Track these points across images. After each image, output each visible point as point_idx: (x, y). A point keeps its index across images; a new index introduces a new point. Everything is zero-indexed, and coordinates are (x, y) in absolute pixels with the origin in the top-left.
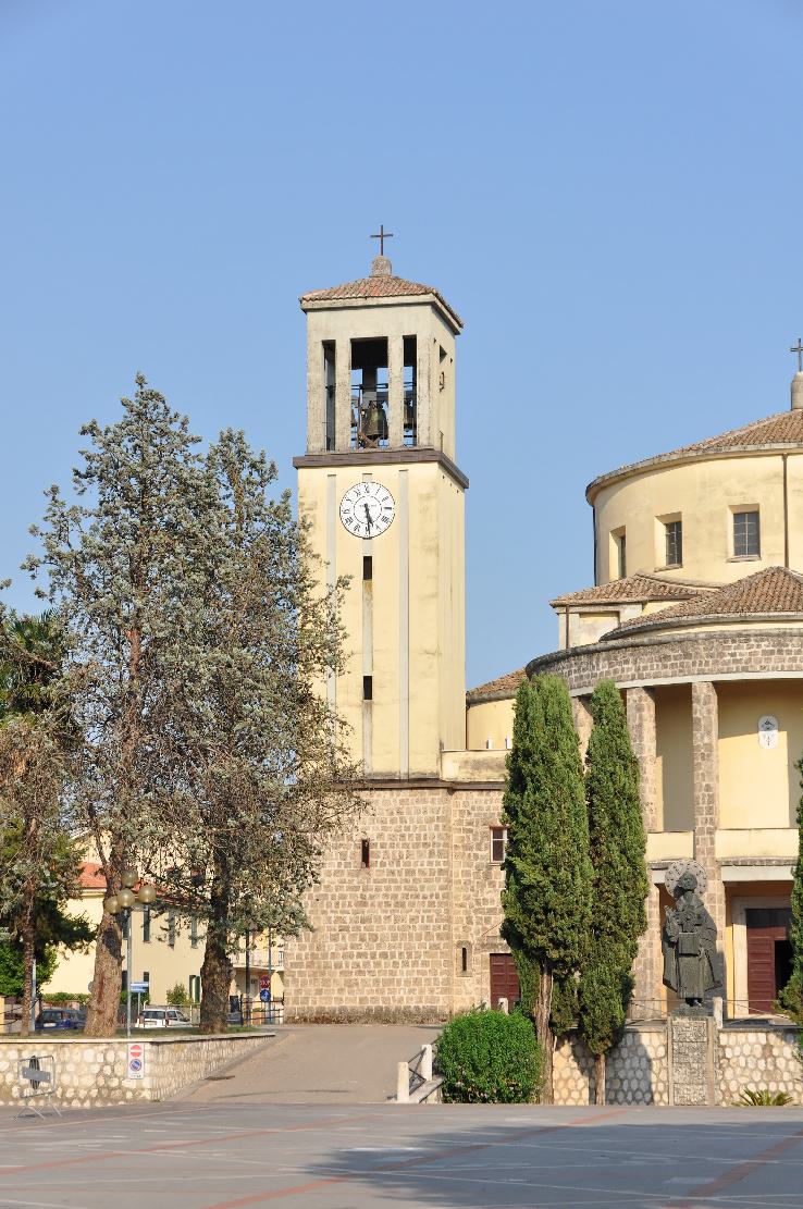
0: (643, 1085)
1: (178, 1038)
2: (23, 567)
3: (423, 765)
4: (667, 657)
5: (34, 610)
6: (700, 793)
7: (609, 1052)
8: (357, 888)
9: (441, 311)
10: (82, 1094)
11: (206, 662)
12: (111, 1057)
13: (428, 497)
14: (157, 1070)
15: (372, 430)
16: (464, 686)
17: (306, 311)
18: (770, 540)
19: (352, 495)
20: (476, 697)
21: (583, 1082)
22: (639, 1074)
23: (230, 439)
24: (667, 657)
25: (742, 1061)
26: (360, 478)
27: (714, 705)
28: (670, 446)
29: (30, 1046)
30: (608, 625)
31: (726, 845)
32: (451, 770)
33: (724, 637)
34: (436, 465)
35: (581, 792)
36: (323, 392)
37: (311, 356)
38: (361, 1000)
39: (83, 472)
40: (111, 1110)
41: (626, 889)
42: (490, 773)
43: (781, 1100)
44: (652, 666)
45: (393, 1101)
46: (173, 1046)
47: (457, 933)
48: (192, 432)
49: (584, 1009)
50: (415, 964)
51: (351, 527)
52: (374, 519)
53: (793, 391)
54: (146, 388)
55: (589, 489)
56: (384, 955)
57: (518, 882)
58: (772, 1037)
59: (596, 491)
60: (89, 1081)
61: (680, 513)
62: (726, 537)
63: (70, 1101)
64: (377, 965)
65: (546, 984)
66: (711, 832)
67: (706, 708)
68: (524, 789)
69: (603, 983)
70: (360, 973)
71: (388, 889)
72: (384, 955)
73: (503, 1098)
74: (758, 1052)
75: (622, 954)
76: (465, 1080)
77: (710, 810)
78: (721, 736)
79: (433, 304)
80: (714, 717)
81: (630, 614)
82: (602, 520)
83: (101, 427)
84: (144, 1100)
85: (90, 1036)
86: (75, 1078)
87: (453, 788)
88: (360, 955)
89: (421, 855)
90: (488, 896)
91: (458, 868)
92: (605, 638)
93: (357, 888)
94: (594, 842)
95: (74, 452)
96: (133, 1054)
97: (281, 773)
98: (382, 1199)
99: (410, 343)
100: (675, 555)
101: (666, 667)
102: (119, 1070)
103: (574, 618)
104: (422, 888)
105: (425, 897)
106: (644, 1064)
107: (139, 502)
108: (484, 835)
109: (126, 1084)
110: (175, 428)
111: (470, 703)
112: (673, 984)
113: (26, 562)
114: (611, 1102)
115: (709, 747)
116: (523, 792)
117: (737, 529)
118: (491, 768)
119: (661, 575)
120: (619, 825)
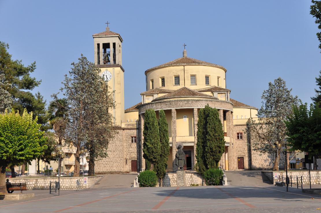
0: (169, 184)
2: (60, 90)
4: (167, 105)
7: (163, 178)
13: (118, 74)
14: (89, 183)
17: (94, 38)
18: (181, 82)
22: (168, 182)
24: (167, 105)
26: (105, 70)
27: (176, 113)
32: (123, 126)
33: (177, 101)
34: (120, 68)
35: (159, 131)
37: (95, 46)
39: (71, 72)
41: (166, 148)
42: (131, 126)
43: (197, 185)
44: (164, 106)
47: (125, 156)
49: (159, 170)
50: (117, 163)
53: (183, 53)
54: (83, 56)
55: (146, 72)
56: (111, 161)
58: (192, 174)
61: (164, 77)
62: (173, 81)
64: (110, 163)
65: (152, 165)
66: (175, 137)
67: (174, 114)
68: (148, 130)
69: (162, 165)
70: (106, 165)
71: (112, 148)
72: (111, 161)
74: (190, 177)
76: (144, 183)
77: (175, 133)
78: (177, 119)
79: (119, 37)
80: (176, 115)
81: (156, 96)
83: (75, 64)
84: (87, 188)
86: (74, 184)
87: (124, 129)
88: (106, 161)
89: (118, 142)
90: (131, 150)
94: (161, 139)
95: (70, 68)
96: (85, 180)
99: (114, 44)
100: (163, 84)
101: (167, 106)
104: (118, 148)
106: (169, 180)
109: (83, 185)
113: (61, 89)
115: (175, 121)
118: (131, 125)
120: (165, 136)
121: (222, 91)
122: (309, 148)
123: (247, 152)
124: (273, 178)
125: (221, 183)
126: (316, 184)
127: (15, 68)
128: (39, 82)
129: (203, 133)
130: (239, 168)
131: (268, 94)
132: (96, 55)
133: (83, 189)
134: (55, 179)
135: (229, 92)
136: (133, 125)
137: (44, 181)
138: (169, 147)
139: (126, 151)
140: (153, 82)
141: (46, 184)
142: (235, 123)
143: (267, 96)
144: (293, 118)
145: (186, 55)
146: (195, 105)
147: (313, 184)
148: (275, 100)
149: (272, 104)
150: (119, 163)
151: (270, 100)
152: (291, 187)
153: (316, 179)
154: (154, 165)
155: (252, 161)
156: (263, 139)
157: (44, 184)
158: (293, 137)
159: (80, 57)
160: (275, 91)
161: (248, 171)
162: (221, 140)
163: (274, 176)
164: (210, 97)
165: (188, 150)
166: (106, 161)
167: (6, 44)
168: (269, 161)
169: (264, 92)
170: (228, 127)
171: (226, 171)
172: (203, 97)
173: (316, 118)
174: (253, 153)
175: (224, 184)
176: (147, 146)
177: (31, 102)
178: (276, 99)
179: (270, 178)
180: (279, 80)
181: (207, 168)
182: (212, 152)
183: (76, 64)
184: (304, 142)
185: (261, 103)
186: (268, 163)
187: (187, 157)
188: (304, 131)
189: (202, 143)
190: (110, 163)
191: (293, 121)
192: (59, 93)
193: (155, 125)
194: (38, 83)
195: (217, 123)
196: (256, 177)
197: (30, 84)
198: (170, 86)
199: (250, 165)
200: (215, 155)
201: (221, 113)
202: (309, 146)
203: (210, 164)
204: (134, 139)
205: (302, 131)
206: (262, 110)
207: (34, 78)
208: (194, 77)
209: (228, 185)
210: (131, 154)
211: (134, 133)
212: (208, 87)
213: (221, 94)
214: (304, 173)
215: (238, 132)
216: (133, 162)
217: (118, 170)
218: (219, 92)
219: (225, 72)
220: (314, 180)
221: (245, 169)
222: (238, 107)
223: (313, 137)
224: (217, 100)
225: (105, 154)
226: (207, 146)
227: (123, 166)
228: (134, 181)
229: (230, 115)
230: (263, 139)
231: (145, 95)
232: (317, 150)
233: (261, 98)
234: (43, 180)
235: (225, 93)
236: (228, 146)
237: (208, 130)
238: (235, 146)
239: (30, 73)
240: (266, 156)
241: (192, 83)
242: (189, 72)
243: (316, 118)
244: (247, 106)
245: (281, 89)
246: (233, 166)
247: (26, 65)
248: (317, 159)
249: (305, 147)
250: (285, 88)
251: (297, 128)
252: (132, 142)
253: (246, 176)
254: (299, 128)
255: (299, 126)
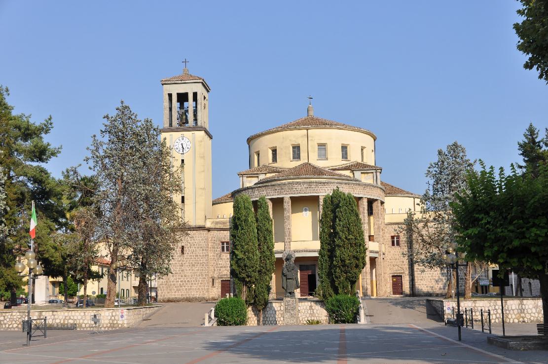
1: (134, 308)
3: (200, 223)
4: (276, 190)
5: (89, 174)
6: (286, 230)
8: (180, 261)
9: (205, 85)
10: (105, 326)
11: (142, 189)
12: (114, 314)
13: (201, 141)
15: (183, 121)
16: (211, 198)
17: (163, 84)
18: (303, 155)
19: (178, 141)
20: (214, 202)
21: (255, 318)
23: (147, 121)
24: (276, 190)
25: (303, 311)
27: (290, 204)
28: (271, 127)
29: (88, 311)
30: (255, 180)
31: (294, 246)
32: (208, 225)
33: (293, 183)
34: (203, 131)
35: (256, 231)
36: (168, 109)
37: (165, 98)
38: (182, 295)
40: (115, 331)
41: (269, 259)
42: (220, 225)
43: (318, 322)
45: (203, 325)
46: (133, 310)
48: (138, 118)
49: (256, 296)
51: (177, 151)
52: (184, 148)
56: (188, 281)
57: (236, 258)
58: (312, 303)
59: (250, 140)
60: (107, 322)
63: (101, 328)
64: (187, 284)
65: (245, 289)
66: (289, 242)
67: (287, 205)
68: (238, 229)
73: (236, 324)
74: (308, 308)
75: (268, 279)
77: (289, 235)
78: (292, 213)
79: (202, 83)
81: (262, 177)
82: (252, 148)
83: (110, 116)
85: (106, 308)
87: (209, 230)
88: (181, 281)
89: (200, 250)
91: (211, 254)
92: (255, 184)
93: (180, 261)
95: (101, 124)
97: (164, 223)
98: (226, 355)
99: (195, 95)
100: (275, 159)
102: (116, 318)
103: (245, 178)
104: (200, 260)
105: (201, 263)
106: (274, 313)
107: (122, 140)
108: (219, 244)
109: (119, 322)
110: (133, 117)
111: (213, 204)
112: (285, 288)
113: (85, 159)
114: (264, 324)
115: (289, 216)
116: (237, 230)
117: (293, 151)
119: (270, 165)
121: (366, 169)
122: (499, 256)
123: (407, 266)
124: (443, 311)
125: (355, 320)
126: (519, 322)
127: (18, 127)
128: (59, 149)
129: (330, 235)
130: (394, 293)
131: (437, 169)
132: (167, 111)
133: (118, 328)
134: (70, 312)
135: (380, 171)
136: (224, 223)
137: (53, 315)
138: (273, 258)
139: (213, 266)
140: (259, 155)
141: (55, 319)
142: (387, 221)
143: (435, 173)
144: (468, 196)
145: (311, 113)
146: (322, 190)
147: (513, 322)
148: (448, 178)
149: (444, 186)
150: (201, 283)
151: (441, 180)
152: (473, 328)
153: (518, 313)
154: (249, 288)
155: (416, 281)
156: (430, 244)
157: (53, 320)
158: (468, 233)
159: (119, 105)
160: (448, 163)
161: (409, 298)
162: (359, 246)
163: (445, 308)
164: (348, 179)
165: (305, 263)
166: (181, 281)
167: (4, 88)
168: (442, 281)
169: (429, 166)
170: (376, 226)
171: (372, 297)
172: (336, 177)
173: (512, 196)
174: (417, 269)
175: (360, 321)
176: (236, 256)
177: (44, 182)
178: (450, 177)
179: (440, 311)
180: (455, 145)
181: (336, 292)
182: (344, 266)
183: (112, 117)
184: (489, 244)
185: (425, 185)
186: (441, 285)
187: (309, 276)
188: (489, 220)
189: (329, 251)
190: (187, 284)
191: (467, 202)
192: (80, 165)
193: (250, 220)
194: (56, 151)
195: (353, 218)
196: (416, 309)
197: (41, 154)
198: (286, 162)
199: (413, 287)
200: (349, 272)
201: (364, 204)
202: (499, 252)
203: (342, 286)
204: (225, 245)
205: (484, 221)
206: (426, 196)
207: (86, 157)
208: (323, 147)
209: (366, 323)
210: (220, 270)
211: (225, 236)
212: (344, 163)
213: (366, 175)
214: (497, 303)
215: (393, 235)
216: (224, 283)
217: (200, 295)
218: (362, 171)
219: (375, 140)
220: (515, 315)
221: (405, 294)
222: (391, 195)
223: (506, 233)
224: (358, 182)
225: (167, 269)
226: (336, 257)
227: (208, 289)
228: (204, 316)
229: (380, 207)
230: (430, 244)
231: (246, 176)
232: (515, 260)
233: (426, 175)
234: (51, 312)
235: (373, 173)
236: (376, 258)
237: (338, 229)
238: (388, 257)
239: (43, 135)
240: (436, 272)
241: (319, 155)
242: (314, 140)
243: (512, 196)
244: (408, 193)
245: (458, 160)
246: (384, 290)
247: (36, 121)
248: (523, 279)
249: (491, 255)
250: (465, 158)
251: (475, 215)
252: (223, 250)
253: (399, 307)
254: (478, 215)
255: (479, 212)
